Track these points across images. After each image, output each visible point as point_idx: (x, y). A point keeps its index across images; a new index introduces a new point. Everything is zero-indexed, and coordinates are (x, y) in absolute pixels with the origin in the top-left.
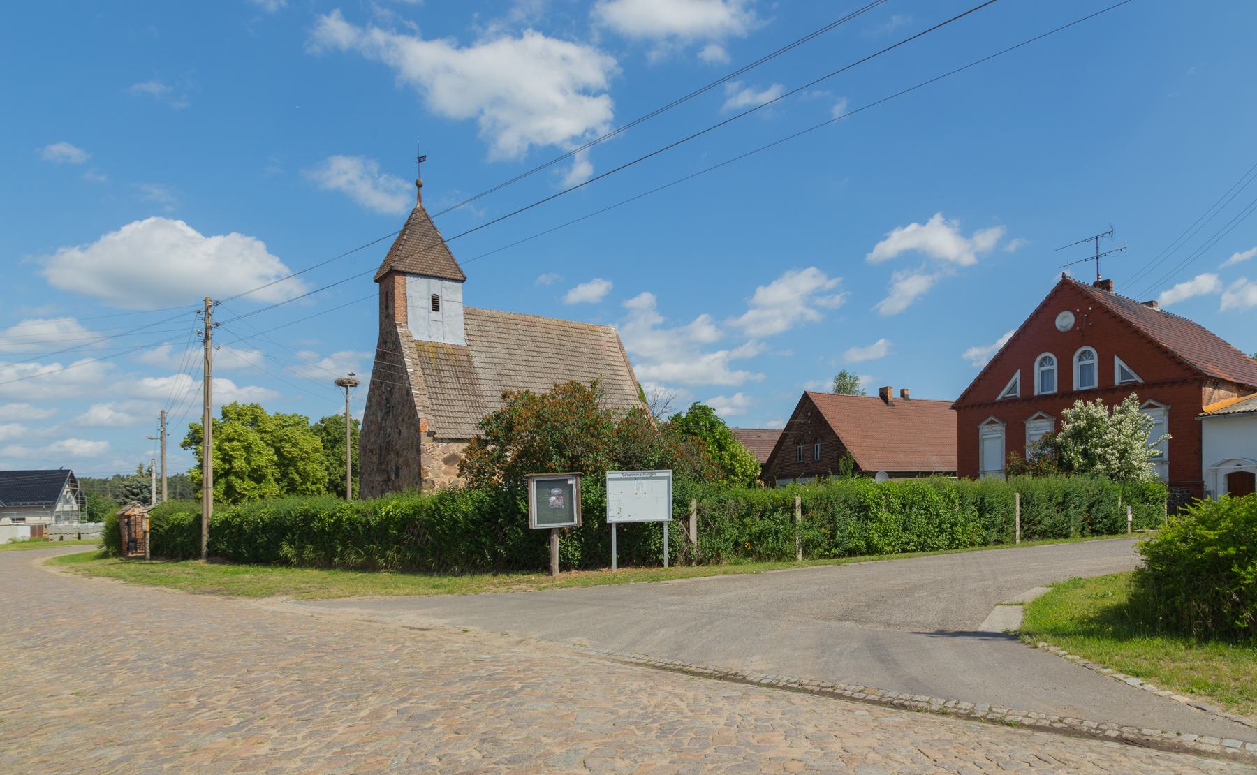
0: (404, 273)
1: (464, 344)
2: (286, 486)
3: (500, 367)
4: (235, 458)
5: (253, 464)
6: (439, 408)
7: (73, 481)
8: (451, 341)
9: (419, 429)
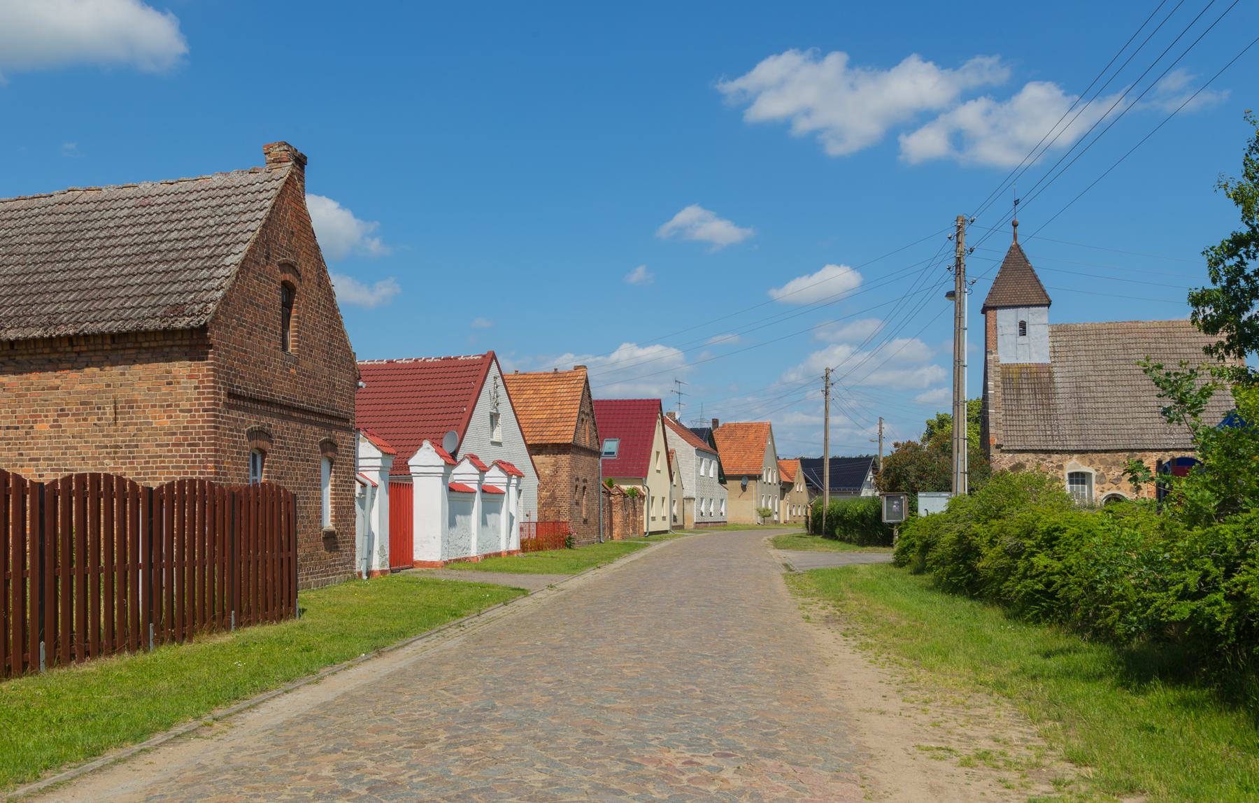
0: (995, 308)
1: (1049, 361)
8: (1036, 360)
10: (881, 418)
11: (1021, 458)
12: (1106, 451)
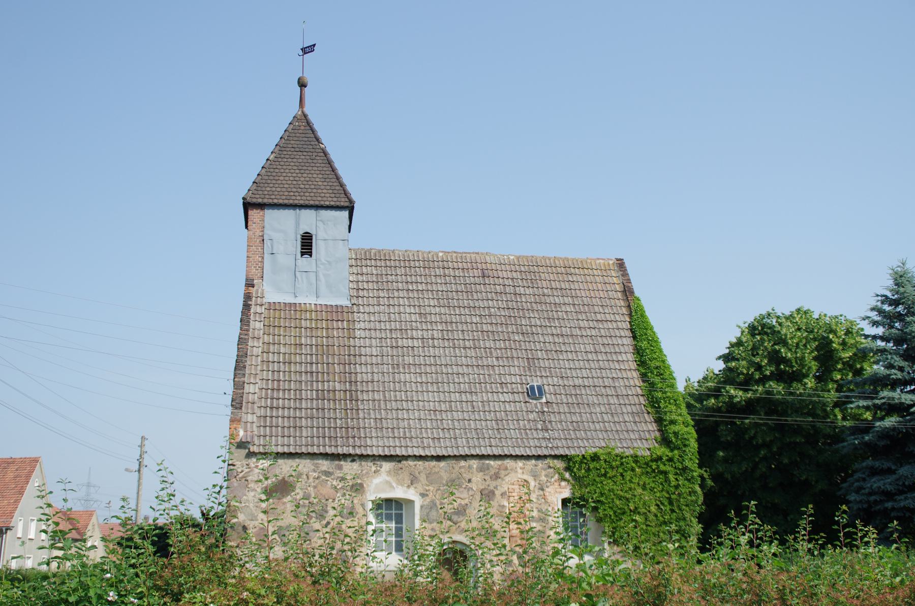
0: (261, 206)
11: (285, 467)
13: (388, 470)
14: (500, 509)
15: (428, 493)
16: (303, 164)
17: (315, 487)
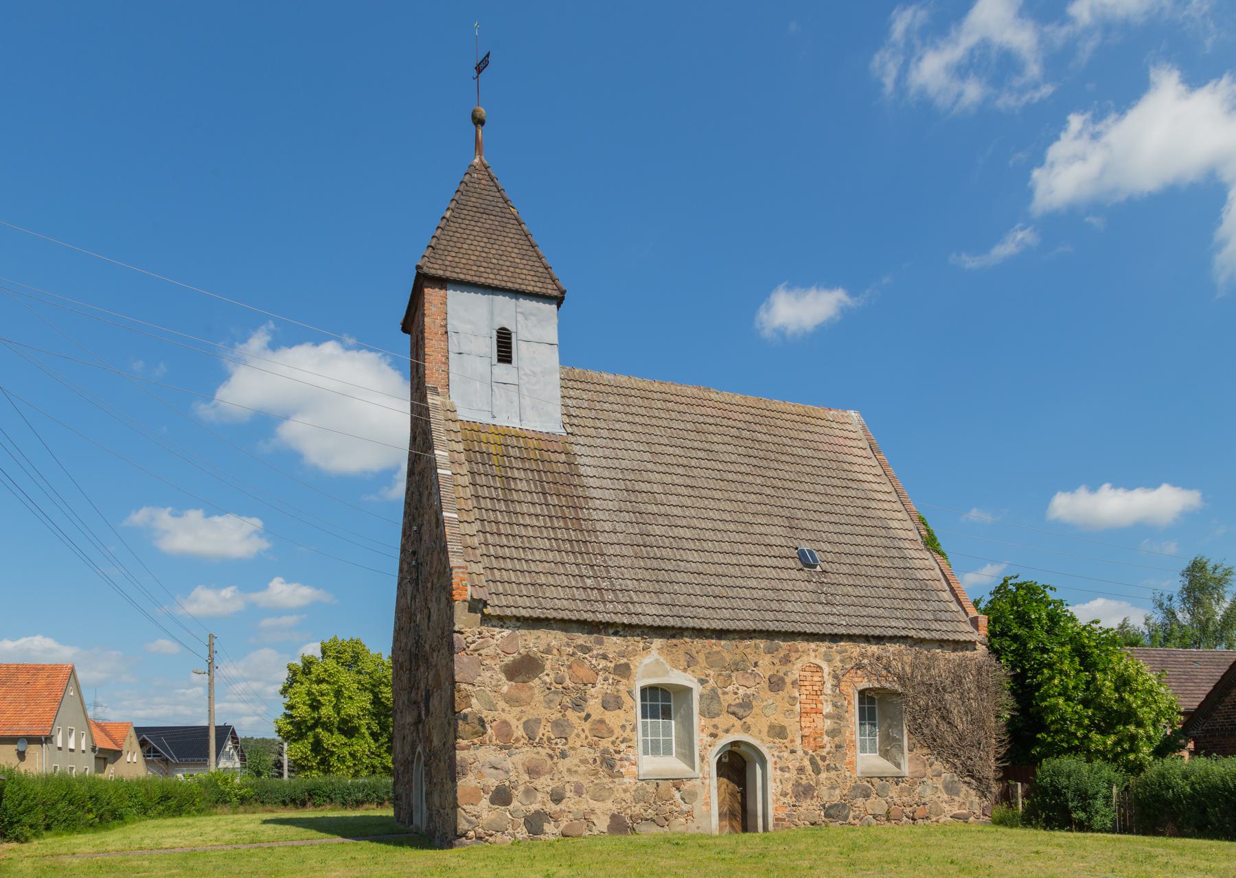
0: (442, 283)
1: (559, 430)
2: (386, 743)
3: (632, 476)
4: (323, 705)
5: (343, 712)
6: (500, 552)
7: (235, 738)
9: (451, 595)
10: (211, 636)
11: (534, 641)
12: (721, 634)
13: (659, 646)
14: (791, 701)
15: (708, 679)
16: (491, 231)
17: (570, 667)
